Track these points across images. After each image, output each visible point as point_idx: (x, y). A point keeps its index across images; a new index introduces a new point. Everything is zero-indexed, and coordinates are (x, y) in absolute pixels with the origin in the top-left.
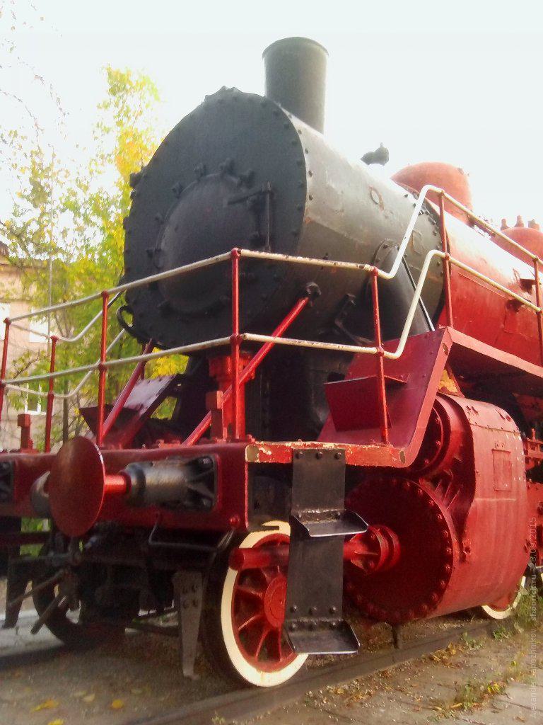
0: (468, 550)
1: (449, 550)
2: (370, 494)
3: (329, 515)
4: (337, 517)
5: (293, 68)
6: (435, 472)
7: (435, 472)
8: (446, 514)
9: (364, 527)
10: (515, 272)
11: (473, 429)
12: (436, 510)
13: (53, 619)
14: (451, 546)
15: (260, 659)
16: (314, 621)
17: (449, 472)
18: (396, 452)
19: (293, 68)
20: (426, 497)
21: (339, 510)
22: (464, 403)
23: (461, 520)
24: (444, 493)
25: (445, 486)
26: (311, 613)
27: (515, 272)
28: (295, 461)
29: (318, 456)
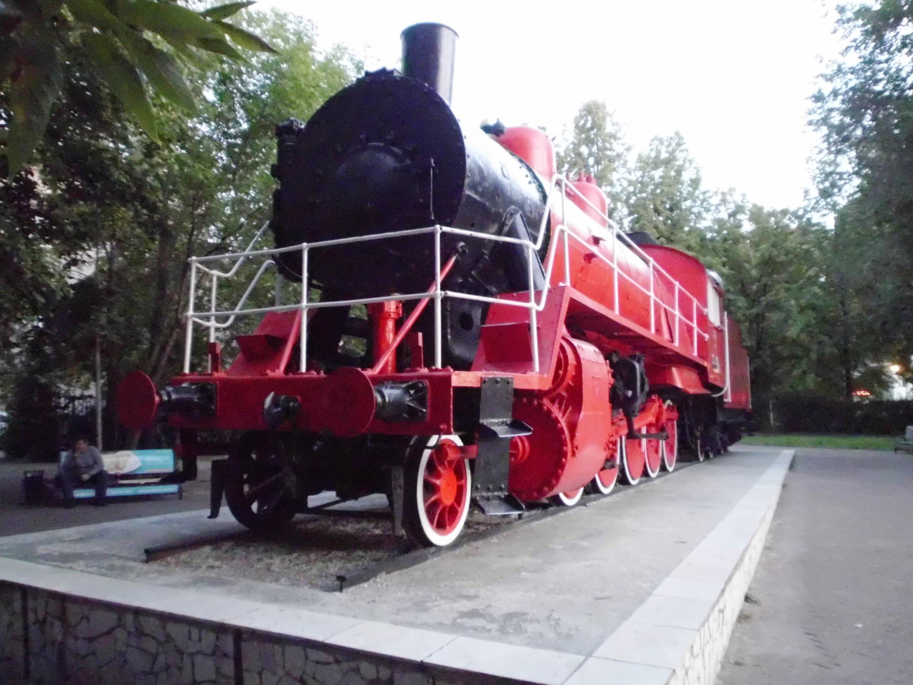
0: (577, 448)
1: (565, 448)
2: (525, 406)
3: (503, 423)
4: (507, 425)
5: (422, 43)
6: (554, 394)
7: (554, 394)
8: (563, 423)
9: (529, 430)
10: (590, 231)
11: (582, 361)
12: (556, 421)
13: (240, 510)
14: (566, 445)
15: (707, 457)
16: (490, 494)
17: (564, 394)
18: (535, 376)
19: (422, 43)
20: (549, 412)
21: (509, 420)
22: (576, 343)
23: (573, 427)
24: (560, 408)
25: (560, 404)
26: (488, 490)
27: (590, 231)
28: (483, 386)
29: (497, 382)
